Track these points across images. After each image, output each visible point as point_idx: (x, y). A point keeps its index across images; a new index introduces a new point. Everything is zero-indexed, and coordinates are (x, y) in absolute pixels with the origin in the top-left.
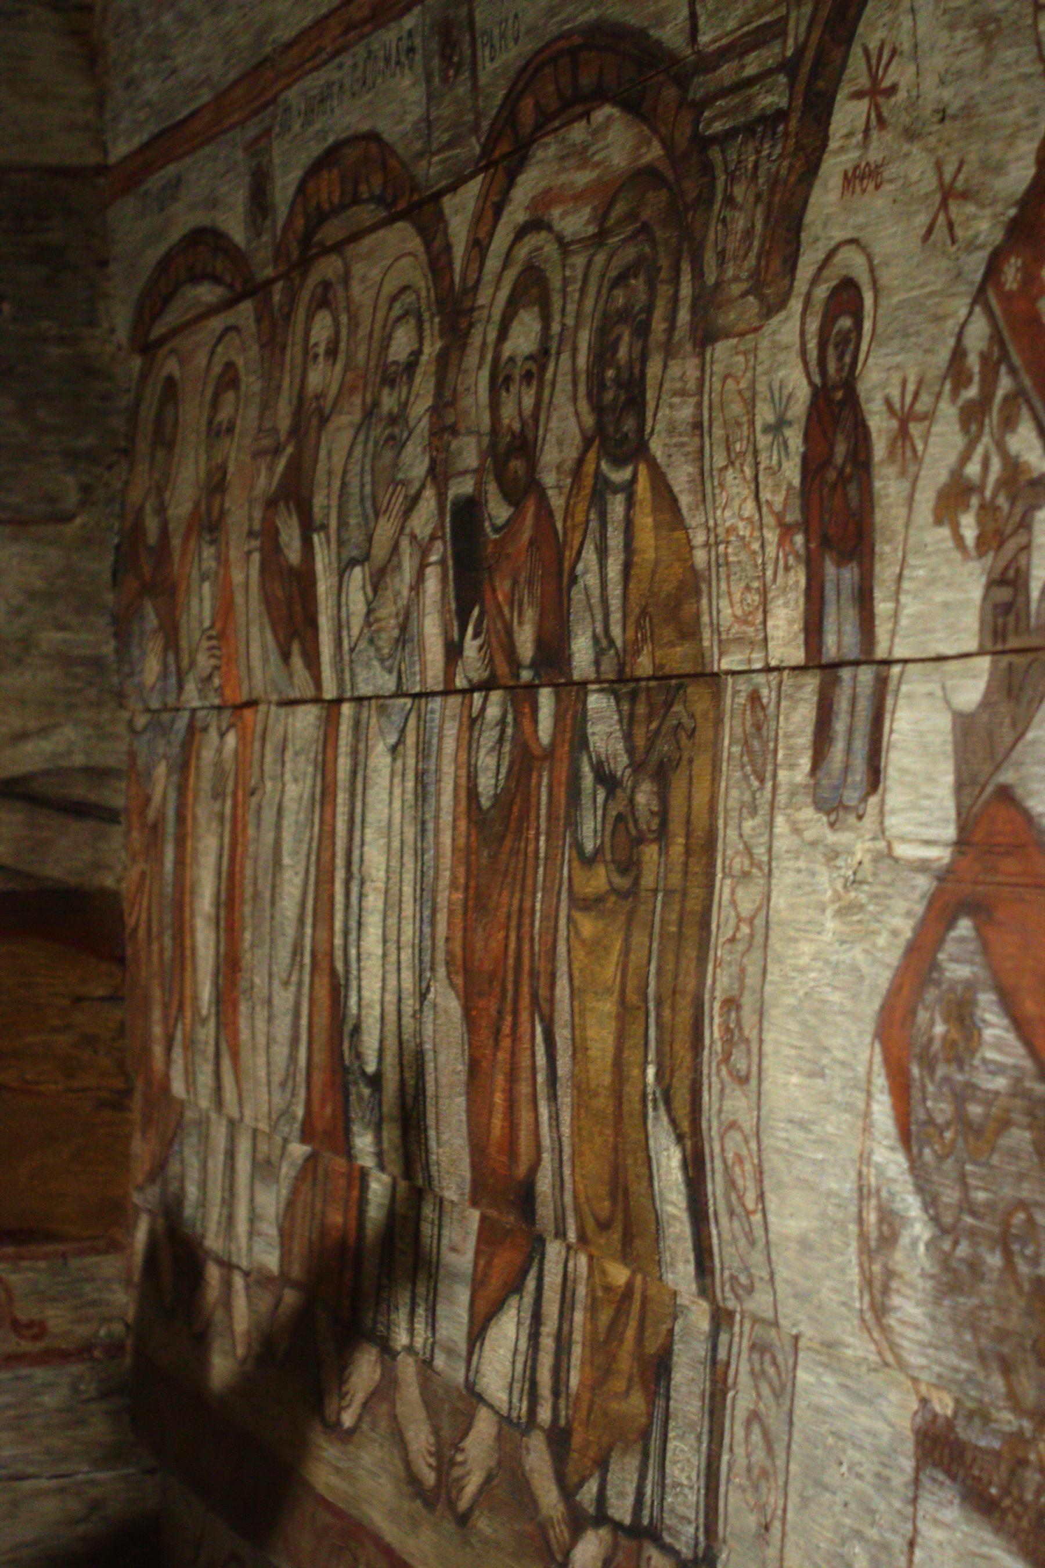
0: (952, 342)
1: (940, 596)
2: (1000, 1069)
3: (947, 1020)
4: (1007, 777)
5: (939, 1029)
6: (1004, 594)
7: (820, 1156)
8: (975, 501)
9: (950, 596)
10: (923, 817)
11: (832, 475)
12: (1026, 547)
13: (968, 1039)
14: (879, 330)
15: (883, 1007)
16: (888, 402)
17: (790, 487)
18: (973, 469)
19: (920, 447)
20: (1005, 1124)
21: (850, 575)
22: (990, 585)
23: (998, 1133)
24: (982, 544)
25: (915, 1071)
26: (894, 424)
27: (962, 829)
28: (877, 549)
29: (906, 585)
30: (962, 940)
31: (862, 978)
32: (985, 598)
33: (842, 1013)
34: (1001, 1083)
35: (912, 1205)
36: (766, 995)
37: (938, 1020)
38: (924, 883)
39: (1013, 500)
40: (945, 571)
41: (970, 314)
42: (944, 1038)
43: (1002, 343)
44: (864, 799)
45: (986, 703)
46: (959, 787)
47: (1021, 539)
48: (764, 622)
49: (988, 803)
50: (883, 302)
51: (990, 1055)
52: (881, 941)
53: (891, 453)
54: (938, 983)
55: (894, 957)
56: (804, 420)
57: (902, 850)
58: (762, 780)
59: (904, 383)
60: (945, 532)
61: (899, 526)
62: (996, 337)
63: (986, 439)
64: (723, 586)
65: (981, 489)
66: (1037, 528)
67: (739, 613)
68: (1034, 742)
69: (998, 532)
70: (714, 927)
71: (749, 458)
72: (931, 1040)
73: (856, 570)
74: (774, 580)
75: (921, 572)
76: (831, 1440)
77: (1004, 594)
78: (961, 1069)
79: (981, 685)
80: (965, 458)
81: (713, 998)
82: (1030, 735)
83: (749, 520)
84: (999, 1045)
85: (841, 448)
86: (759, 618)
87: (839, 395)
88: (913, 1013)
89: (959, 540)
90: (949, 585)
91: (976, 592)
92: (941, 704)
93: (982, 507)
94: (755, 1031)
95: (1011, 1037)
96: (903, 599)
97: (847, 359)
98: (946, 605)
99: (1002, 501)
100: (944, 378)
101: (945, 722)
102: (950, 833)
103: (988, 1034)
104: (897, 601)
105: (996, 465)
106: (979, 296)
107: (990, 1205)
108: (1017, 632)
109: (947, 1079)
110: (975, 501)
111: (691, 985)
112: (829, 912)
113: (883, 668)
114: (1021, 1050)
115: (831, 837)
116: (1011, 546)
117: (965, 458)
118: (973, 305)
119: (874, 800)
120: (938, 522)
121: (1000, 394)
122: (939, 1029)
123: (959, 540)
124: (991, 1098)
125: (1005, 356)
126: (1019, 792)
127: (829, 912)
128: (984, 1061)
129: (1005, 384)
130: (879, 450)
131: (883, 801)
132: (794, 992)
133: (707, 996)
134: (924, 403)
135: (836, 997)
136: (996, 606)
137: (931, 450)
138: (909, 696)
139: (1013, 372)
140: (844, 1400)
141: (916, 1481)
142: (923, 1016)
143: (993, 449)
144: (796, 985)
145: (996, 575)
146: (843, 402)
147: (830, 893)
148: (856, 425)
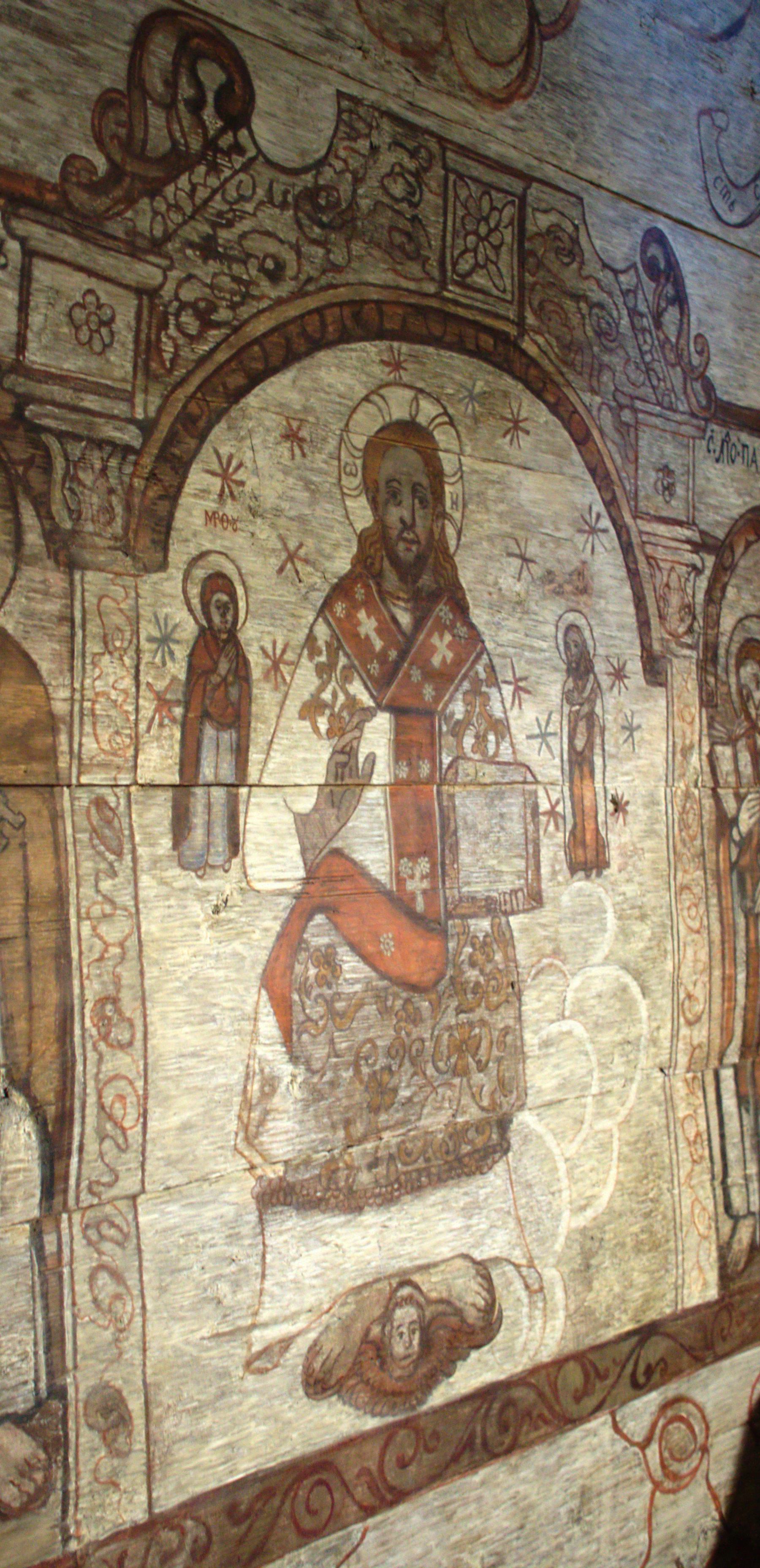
0: (307, 631)
1: (301, 755)
2: (357, 981)
3: (316, 967)
4: (337, 844)
5: (312, 972)
6: (342, 758)
7: (211, 1067)
8: (328, 712)
9: (308, 756)
10: (280, 867)
11: (215, 679)
12: (359, 738)
13: (333, 972)
14: (251, 607)
15: (265, 970)
16: (263, 649)
17: (174, 679)
18: (326, 696)
19: (288, 679)
20: (361, 1005)
21: (228, 737)
22: (334, 753)
23: (356, 1012)
24: (330, 733)
25: (296, 997)
26: (269, 662)
27: (308, 870)
28: (253, 725)
29: (275, 746)
30: (319, 925)
31: (243, 958)
32: (330, 759)
33: (227, 981)
34: (358, 987)
35: (285, 1069)
36: (147, 987)
37: (310, 966)
38: (286, 902)
39: (352, 715)
40: (305, 743)
41: (316, 620)
42: (317, 975)
43: (338, 640)
44: (229, 861)
45: (315, 809)
46: (303, 852)
47: (356, 733)
48: (136, 757)
49: (325, 857)
50: (253, 597)
51: (348, 976)
52: (257, 935)
53: (266, 676)
54: (307, 949)
55: (269, 942)
56: (191, 643)
57: (257, 886)
58: (120, 854)
59: (274, 643)
60: (307, 723)
61: (273, 716)
62: (334, 635)
63: (333, 683)
64: (88, 728)
65: (332, 707)
66: (366, 730)
67: (107, 748)
68: (353, 827)
69: (341, 728)
70: (75, 955)
71: (132, 653)
72: (307, 979)
73: (234, 735)
74: (148, 730)
75: (285, 742)
76: (182, 1241)
77: (342, 758)
78: (330, 987)
79: (313, 800)
80: (321, 689)
81: (83, 1002)
82: (350, 824)
83: (125, 692)
84: (354, 970)
85: (224, 666)
86: (131, 752)
87: (224, 636)
88: (291, 968)
89: (316, 730)
90: (307, 750)
91: (326, 755)
92: (284, 809)
93: (332, 715)
94: (138, 1013)
95: (361, 965)
96: (272, 754)
97: (229, 618)
98: (305, 760)
99: (345, 714)
100: (303, 648)
101: (289, 818)
102: (301, 873)
103: (345, 967)
104: (268, 754)
105: (341, 698)
106: (321, 612)
107: (349, 1048)
108: (351, 776)
109: (320, 995)
110: (328, 712)
111: (54, 997)
112: (204, 926)
113: (233, 790)
114: (367, 969)
115: (200, 884)
116: (348, 737)
117: (321, 689)
118: (318, 616)
119: (236, 861)
120: (302, 717)
121: (340, 665)
122: (312, 972)
123: (316, 730)
124: (350, 997)
125: (340, 647)
126: (346, 851)
127: (204, 926)
128: (345, 980)
129: (342, 661)
130: (256, 673)
131: (243, 860)
132: (178, 979)
133: (76, 1002)
134: (290, 656)
135: (221, 973)
136: (337, 763)
137: (296, 680)
138: (258, 805)
139: (347, 655)
140: (191, 1212)
141: (261, 1220)
142: (298, 968)
143: (338, 689)
144: (179, 974)
145: (339, 748)
146: (226, 642)
147: (202, 916)
148: (237, 655)
